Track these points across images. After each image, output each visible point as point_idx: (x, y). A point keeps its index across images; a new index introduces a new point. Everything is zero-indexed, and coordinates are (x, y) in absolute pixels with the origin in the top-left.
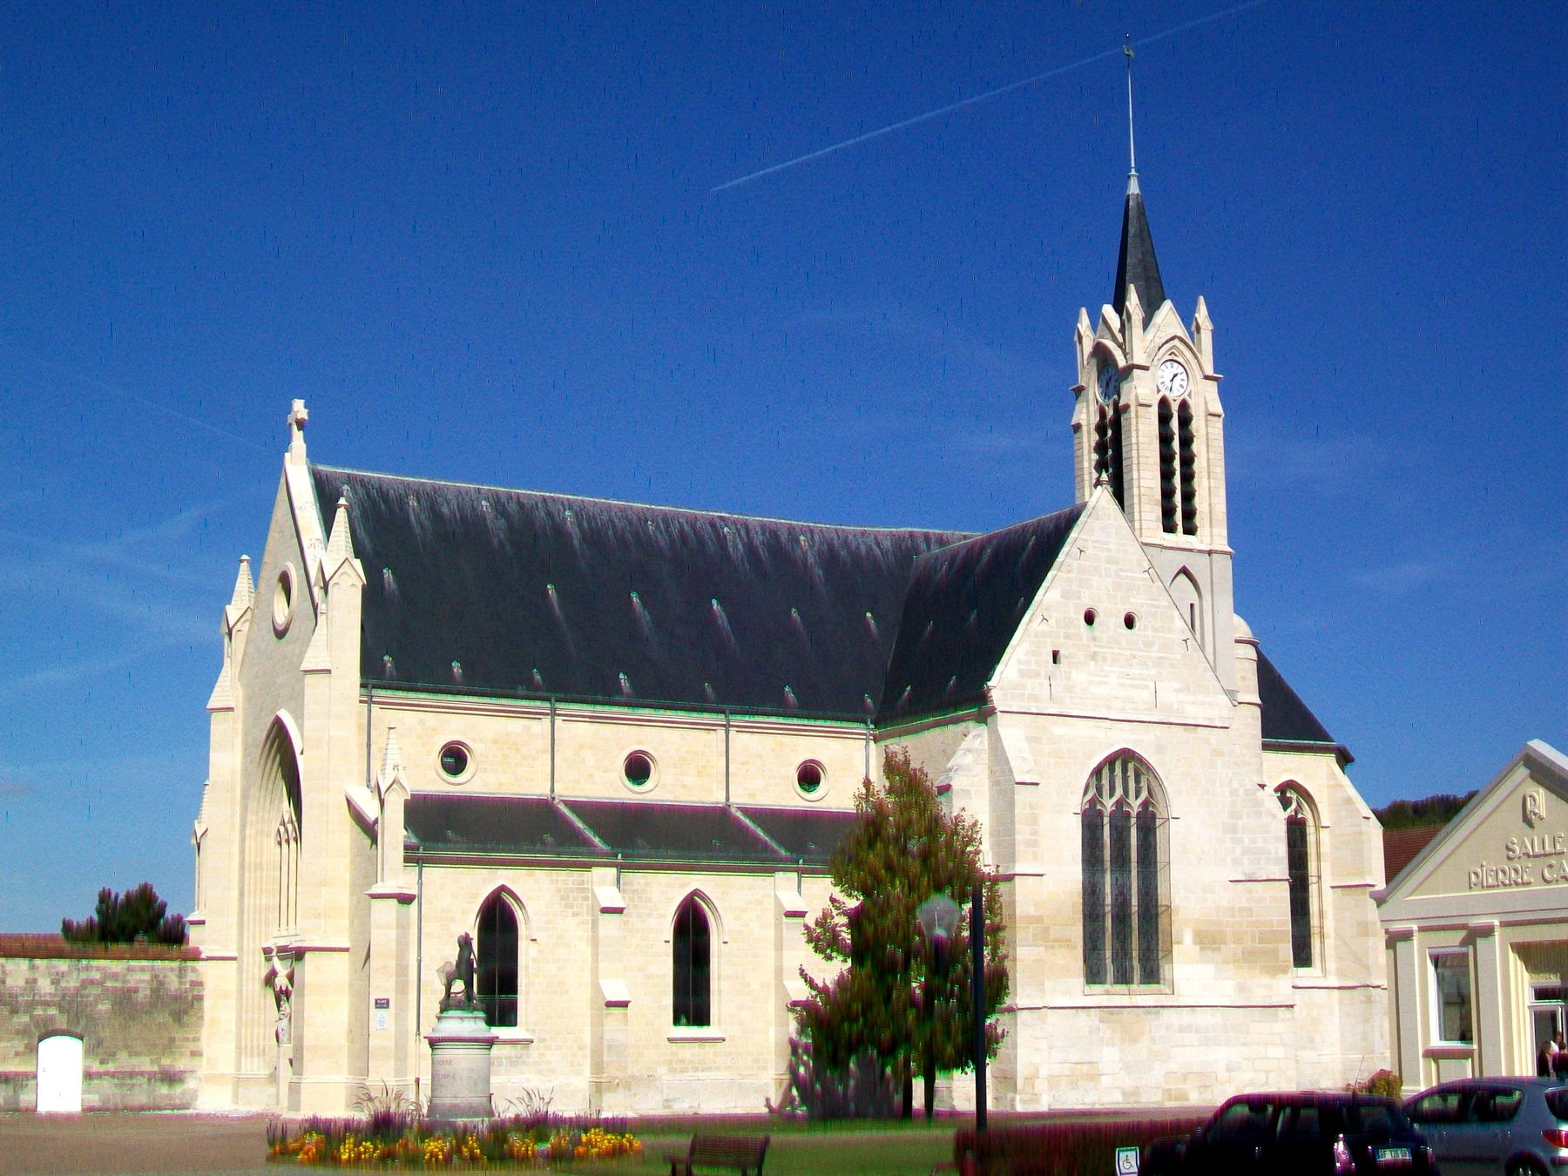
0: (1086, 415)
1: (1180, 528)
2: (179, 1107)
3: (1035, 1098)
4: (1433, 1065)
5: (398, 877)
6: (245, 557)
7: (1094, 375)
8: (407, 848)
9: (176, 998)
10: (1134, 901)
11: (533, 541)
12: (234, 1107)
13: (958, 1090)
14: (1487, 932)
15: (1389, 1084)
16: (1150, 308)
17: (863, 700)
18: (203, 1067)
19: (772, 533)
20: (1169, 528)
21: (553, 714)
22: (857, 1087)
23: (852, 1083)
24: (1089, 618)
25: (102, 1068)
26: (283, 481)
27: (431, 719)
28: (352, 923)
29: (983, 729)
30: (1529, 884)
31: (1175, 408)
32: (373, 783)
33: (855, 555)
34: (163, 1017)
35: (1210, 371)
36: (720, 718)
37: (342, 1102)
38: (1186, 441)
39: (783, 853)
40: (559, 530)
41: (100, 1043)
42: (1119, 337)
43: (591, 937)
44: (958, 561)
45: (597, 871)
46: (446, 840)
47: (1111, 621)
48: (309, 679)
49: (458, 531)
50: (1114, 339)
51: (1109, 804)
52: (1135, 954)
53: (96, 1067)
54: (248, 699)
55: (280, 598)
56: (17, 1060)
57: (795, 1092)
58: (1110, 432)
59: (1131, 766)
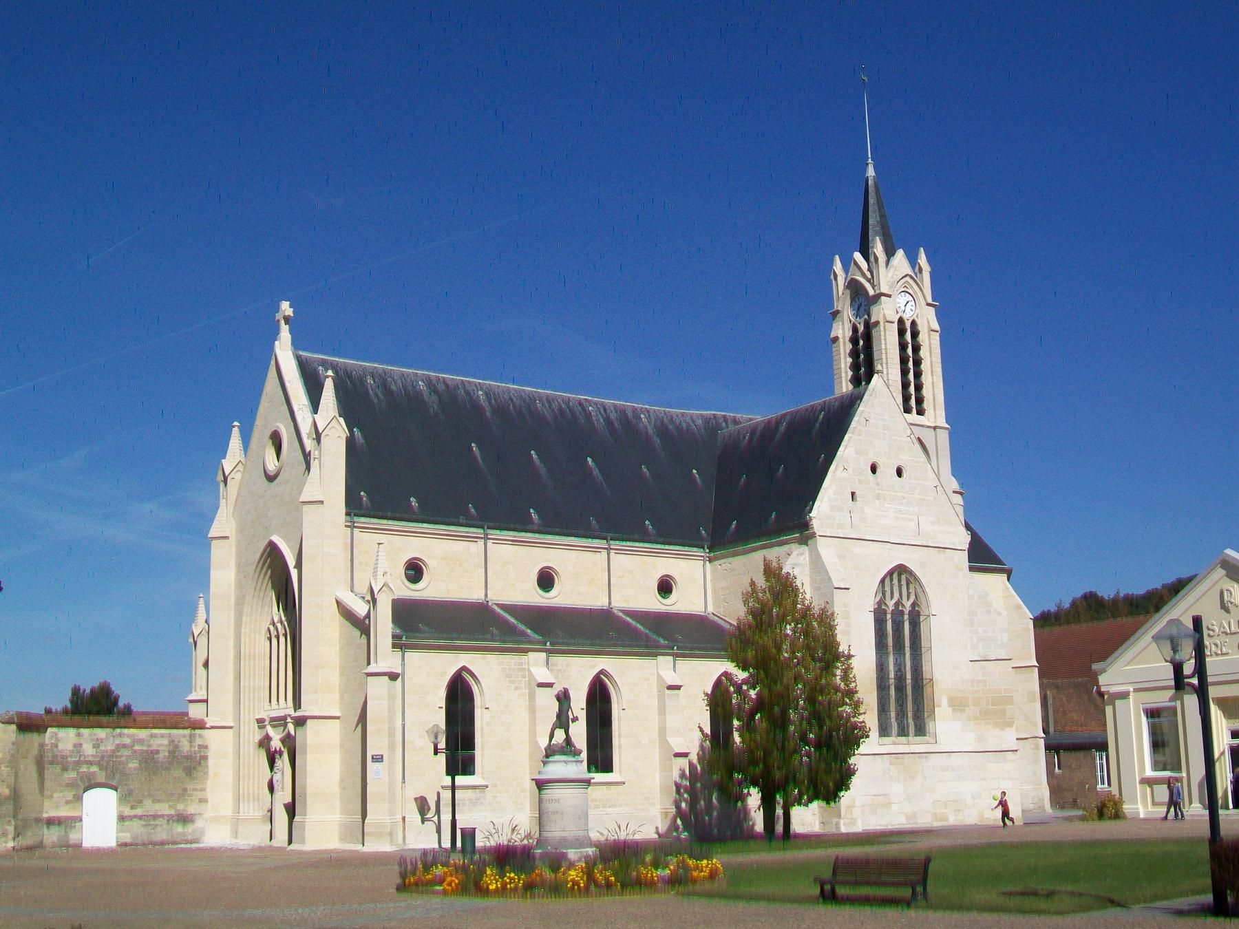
0: (842, 331)
1: (914, 410)
2: (191, 842)
3: (853, 822)
4: (1148, 789)
5: (387, 658)
6: (236, 423)
7: (848, 301)
8: (394, 637)
9: (189, 757)
10: (909, 676)
11: (458, 410)
12: (234, 841)
13: (807, 818)
14: (1124, 695)
15: (1115, 804)
16: (890, 253)
17: (699, 531)
18: (208, 811)
19: (622, 412)
20: (907, 410)
21: (486, 538)
22: (718, 816)
23: (715, 814)
24: (874, 469)
25: (133, 813)
26: (273, 362)
27: (397, 540)
28: (342, 697)
29: (804, 549)
30: (1227, 654)
31: (908, 325)
32: (364, 590)
33: (678, 428)
34: (178, 773)
35: (930, 300)
36: (603, 543)
37: (336, 836)
38: (916, 349)
39: (662, 641)
40: (476, 407)
41: (130, 793)
42: (869, 275)
43: (519, 696)
44: (758, 433)
45: (532, 655)
46: (419, 631)
47: (887, 471)
48: (306, 508)
49: (404, 403)
50: (864, 275)
51: (891, 604)
52: (910, 714)
53: (128, 812)
54: (241, 530)
55: (270, 453)
56: (67, 807)
57: (679, 822)
58: (861, 342)
59: (903, 577)
